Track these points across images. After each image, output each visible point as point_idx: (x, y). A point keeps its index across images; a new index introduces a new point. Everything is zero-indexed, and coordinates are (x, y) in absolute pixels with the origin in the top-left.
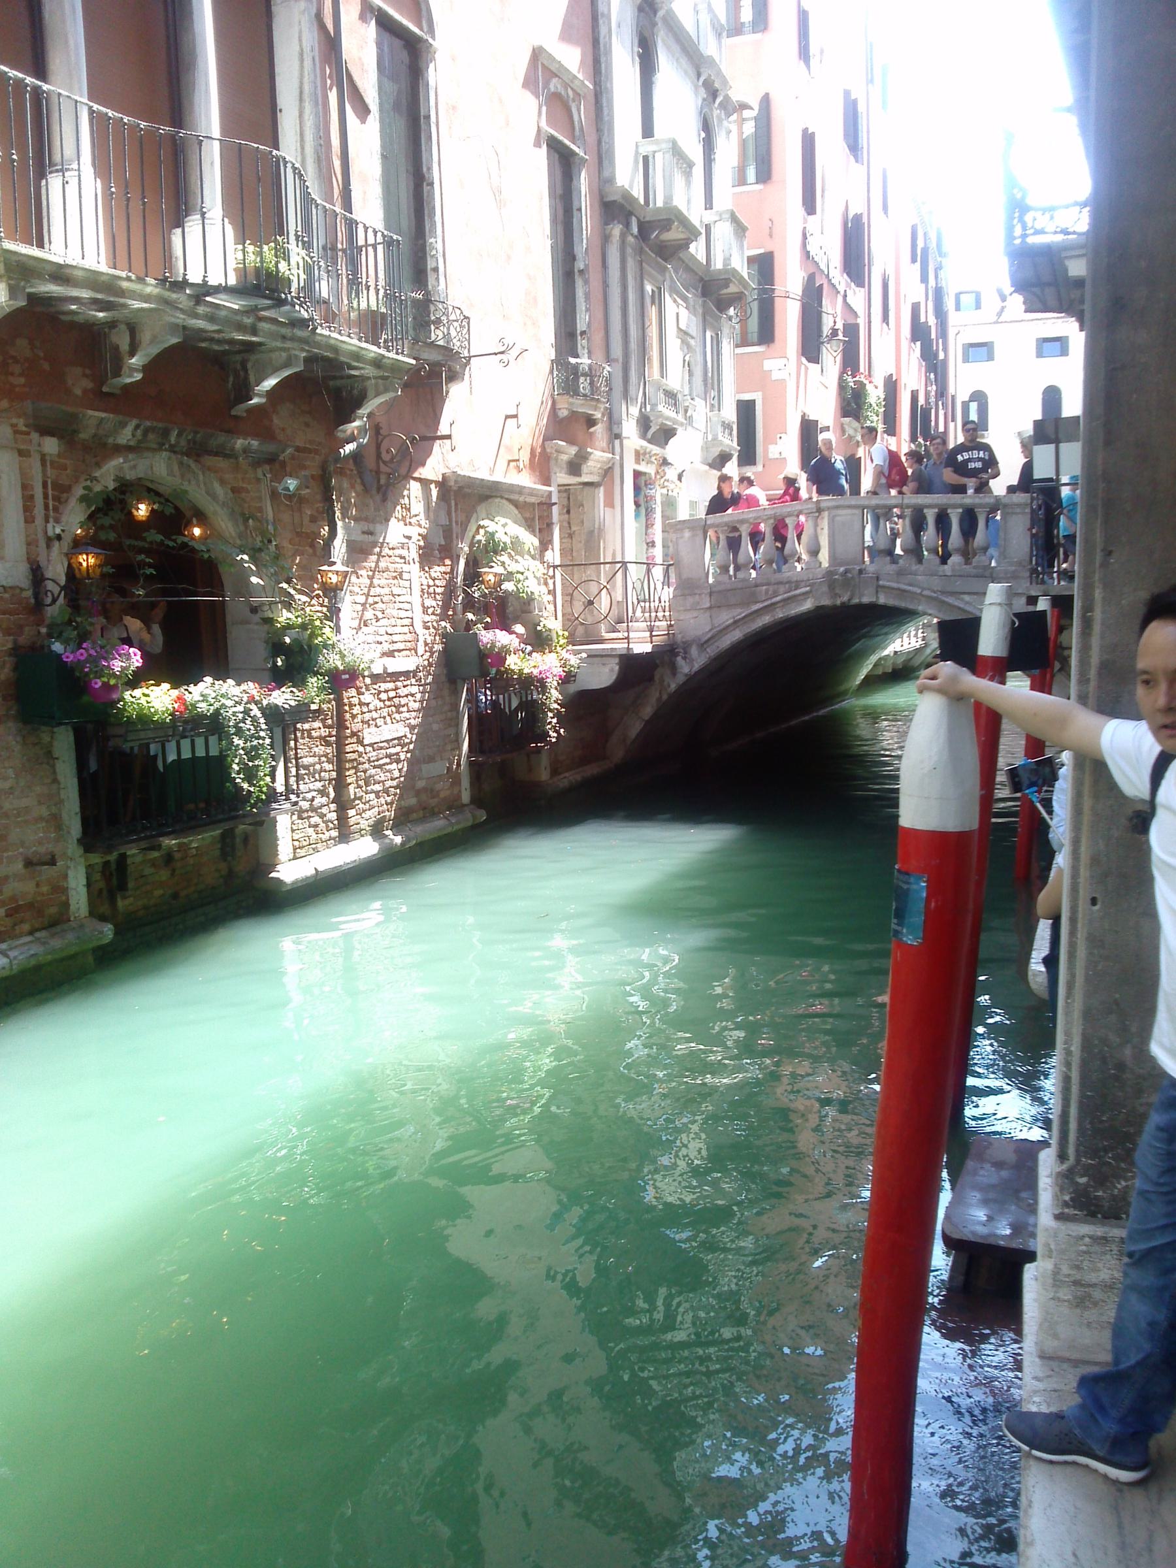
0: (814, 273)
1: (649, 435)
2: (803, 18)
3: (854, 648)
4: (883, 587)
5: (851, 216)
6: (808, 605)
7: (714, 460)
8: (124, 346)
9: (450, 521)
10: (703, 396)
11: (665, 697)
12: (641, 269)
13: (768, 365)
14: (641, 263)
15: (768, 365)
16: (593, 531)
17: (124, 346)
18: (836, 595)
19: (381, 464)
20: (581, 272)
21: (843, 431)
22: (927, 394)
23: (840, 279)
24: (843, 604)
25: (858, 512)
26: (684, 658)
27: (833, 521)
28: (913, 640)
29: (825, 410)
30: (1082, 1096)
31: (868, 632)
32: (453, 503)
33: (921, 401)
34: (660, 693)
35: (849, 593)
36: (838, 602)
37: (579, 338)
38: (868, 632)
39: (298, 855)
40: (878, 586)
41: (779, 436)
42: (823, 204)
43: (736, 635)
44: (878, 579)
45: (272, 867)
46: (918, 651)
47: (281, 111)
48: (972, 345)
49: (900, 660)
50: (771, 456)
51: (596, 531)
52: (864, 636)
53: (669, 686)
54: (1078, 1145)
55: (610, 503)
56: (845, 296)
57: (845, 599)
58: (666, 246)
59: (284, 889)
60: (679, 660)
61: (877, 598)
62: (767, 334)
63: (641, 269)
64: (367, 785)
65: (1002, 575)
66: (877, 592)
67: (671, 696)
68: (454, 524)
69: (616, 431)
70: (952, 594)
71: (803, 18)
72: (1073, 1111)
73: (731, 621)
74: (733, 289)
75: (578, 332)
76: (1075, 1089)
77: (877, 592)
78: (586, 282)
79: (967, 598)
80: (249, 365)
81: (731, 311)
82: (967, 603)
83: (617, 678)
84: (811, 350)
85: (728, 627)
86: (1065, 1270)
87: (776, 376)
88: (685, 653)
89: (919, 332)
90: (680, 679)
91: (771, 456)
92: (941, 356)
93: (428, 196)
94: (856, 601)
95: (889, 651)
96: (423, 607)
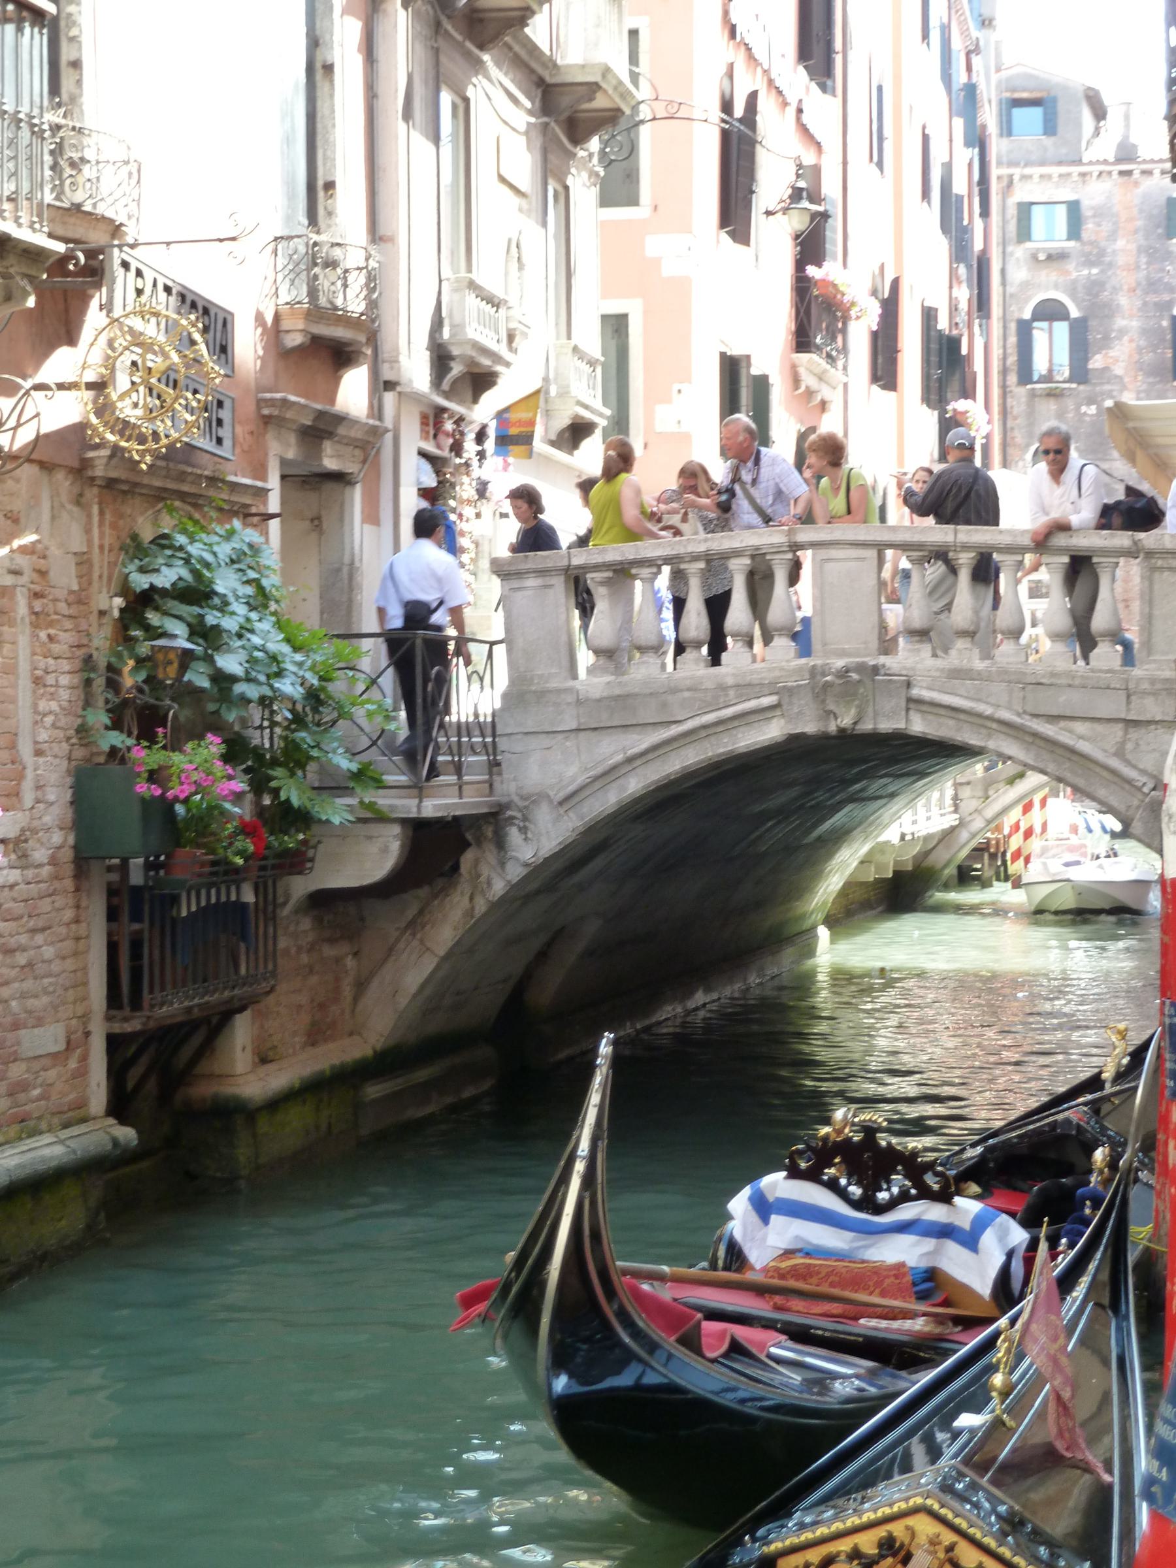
1: (446, 385)
3: (827, 825)
4: (919, 701)
6: (772, 732)
7: (561, 434)
9: (90, 542)
11: (481, 907)
12: (437, 64)
14: (436, 52)
16: (339, 570)
18: (830, 714)
21: (796, 381)
22: (953, 309)
24: (842, 731)
25: (872, 554)
26: (523, 830)
27: (821, 567)
28: (935, 811)
31: (863, 790)
32: (95, 509)
33: (943, 324)
34: (471, 899)
35: (853, 711)
36: (832, 728)
38: (863, 790)
40: (910, 700)
43: (635, 785)
44: (909, 685)
46: (948, 834)
49: (908, 857)
50: (659, 427)
51: (345, 570)
52: (853, 799)
53: (489, 883)
55: (372, 517)
56: (800, 111)
57: (846, 721)
58: (481, 21)
59: (136, 1142)
60: (514, 835)
61: (908, 720)
63: (437, 64)
65: (1146, 686)
66: (908, 710)
67: (495, 906)
68: (96, 550)
69: (387, 374)
70: (1053, 718)
73: (619, 757)
74: (600, 102)
77: (908, 710)
79: (1080, 727)
81: (594, 144)
82: (1081, 737)
83: (397, 864)
85: (614, 768)
87: (669, 269)
88: (525, 819)
90: (515, 872)
91: (659, 427)
94: (867, 726)
95: (891, 835)
96: (36, 712)
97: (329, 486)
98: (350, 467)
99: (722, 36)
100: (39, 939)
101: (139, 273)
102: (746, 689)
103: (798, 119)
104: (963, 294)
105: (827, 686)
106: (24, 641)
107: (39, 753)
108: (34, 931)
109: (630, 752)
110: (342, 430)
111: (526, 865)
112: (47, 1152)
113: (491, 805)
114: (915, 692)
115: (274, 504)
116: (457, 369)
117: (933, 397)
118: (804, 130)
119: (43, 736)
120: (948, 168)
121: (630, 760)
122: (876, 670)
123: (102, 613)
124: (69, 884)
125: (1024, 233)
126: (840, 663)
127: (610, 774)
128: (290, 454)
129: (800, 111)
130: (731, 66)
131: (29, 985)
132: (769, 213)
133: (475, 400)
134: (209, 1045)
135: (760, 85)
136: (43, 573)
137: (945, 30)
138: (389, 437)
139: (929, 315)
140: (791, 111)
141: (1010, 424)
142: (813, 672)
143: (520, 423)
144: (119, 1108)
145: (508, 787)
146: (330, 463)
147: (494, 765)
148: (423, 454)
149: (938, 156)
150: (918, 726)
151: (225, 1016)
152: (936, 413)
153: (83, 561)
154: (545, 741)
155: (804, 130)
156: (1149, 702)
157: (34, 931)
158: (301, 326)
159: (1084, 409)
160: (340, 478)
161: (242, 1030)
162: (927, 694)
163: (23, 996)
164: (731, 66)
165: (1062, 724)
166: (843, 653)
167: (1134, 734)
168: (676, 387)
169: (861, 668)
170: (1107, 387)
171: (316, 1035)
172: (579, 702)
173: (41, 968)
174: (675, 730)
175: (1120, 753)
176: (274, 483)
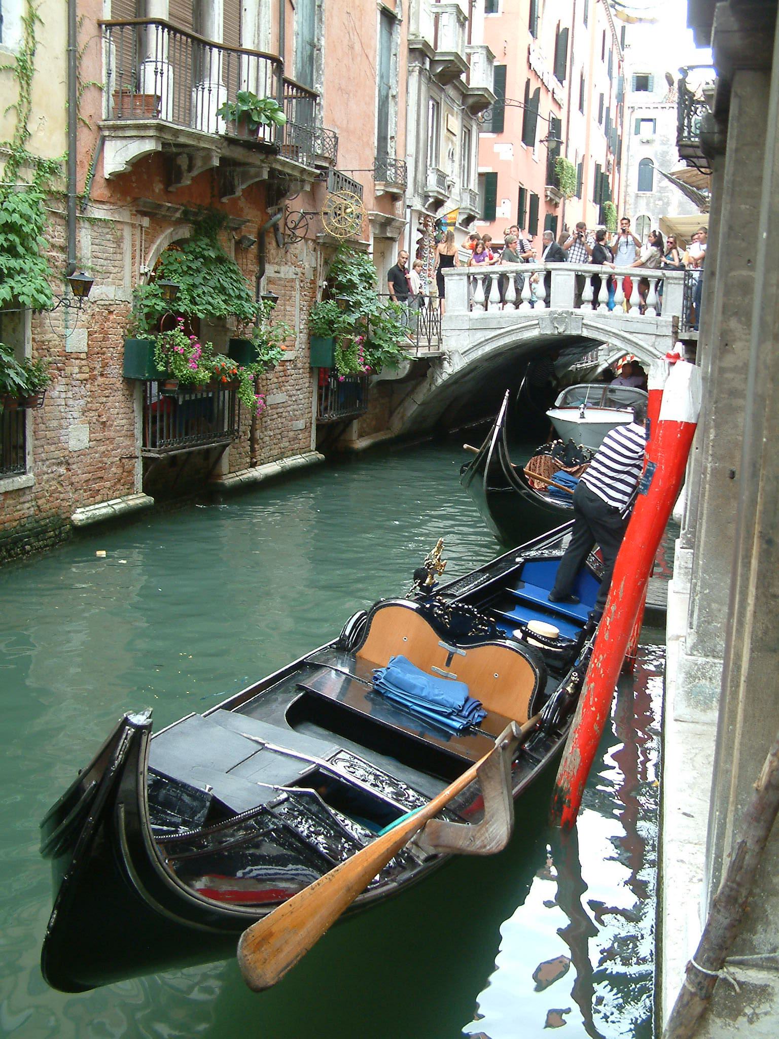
0: (539, 88)
2: (603, 58)
5: (561, 30)
8: (185, 167)
10: (143, 27)
11: (433, 388)
13: (497, 148)
14: (437, 105)
15: (497, 148)
17: (185, 167)
19: (287, 228)
20: (394, 97)
22: (609, 163)
23: (551, 81)
26: (449, 363)
29: (538, 185)
30: (690, 509)
32: (319, 253)
33: (603, 170)
35: (564, 327)
36: (556, 332)
37: (389, 140)
39: (231, 471)
40: (583, 324)
41: (503, 201)
42: (627, 172)
43: (488, 348)
45: (220, 476)
47: (245, 10)
48: (643, 120)
54: (689, 524)
56: (553, 93)
57: (561, 330)
62: (498, 127)
64: (266, 430)
65: (663, 323)
71: (603, 58)
72: (688, 514)
73: (483, 339)
75: (389, 137)
76: (688, 507)
78: (396, 104)
79: (640, 336)
80: (235, 174)
84: (528, 137)
86: (683, 563)
89: (603, 116)
90: (445, 377)
92: (619, 133)
93: (317, 57)
97: (388, 241)
98: (395, 236)
99: (526, 66)
100: (299, 392)
101: (338, 177)
102: (528, 318)
103: (553, 96)
104: (611, 158)
105: (556, 318)
106: (298, 296)
107: (301, 332)
108: (297, 390)
109: (487, 338)
110: (393, 223)
111: (449, 375)
112: (299, 460)
113: (439, 353)
114: (585, 321)
115: (371, 250)
116: (431, 200)
117: (598, 199)
118: (554, 99)
119: (302, 327)
120: (608, 109)
121: (487, 340)
122: (572, 313)
123: (320, 287)
124: (307, 375)
125: (637, 132)
126: (560, 311)
127: (480, 344)
128: (377, 232)
129: (553, 93)
130: (529, 80)
131: (295, 407)
132: (541, 141)
133: (436, 211)
134: (343, 431)
135: (539, 85)
136: (303, 274)
137: (611, 53)
138: (408, 226)
139: (598, 167)
140: (550, 94)
141: (627, 207)
142: (551, 313)
143: (451, 218)
144: (318, 449)
145: (444, 348)
146: (389, 235)
147: (440, 340)
148: (418, 230)
149: (606, 104)
150: (585, 333)
151: (225, 447)
152: (598, 206)
153: (315, 269)
154: (458, 332)
155: (554, 99)
156: (664, 329)
157: (297, 390)
158: (383, 188)
159: (657, 202)
160: (392, 239)
161: (356, 425)
162: (589, 323)
163: (294, 410)
164: (529, 80)
165: (635, 334)
166: (561, 307)
167: (659, 339)
168: (503, 201)
169: (567, 312)
170: (666, 194)
171: (377, 430)
172: (470, 320)
173: (299, 402)
174: (502, 331)
175: (653, 346)
176: (371, 242)
